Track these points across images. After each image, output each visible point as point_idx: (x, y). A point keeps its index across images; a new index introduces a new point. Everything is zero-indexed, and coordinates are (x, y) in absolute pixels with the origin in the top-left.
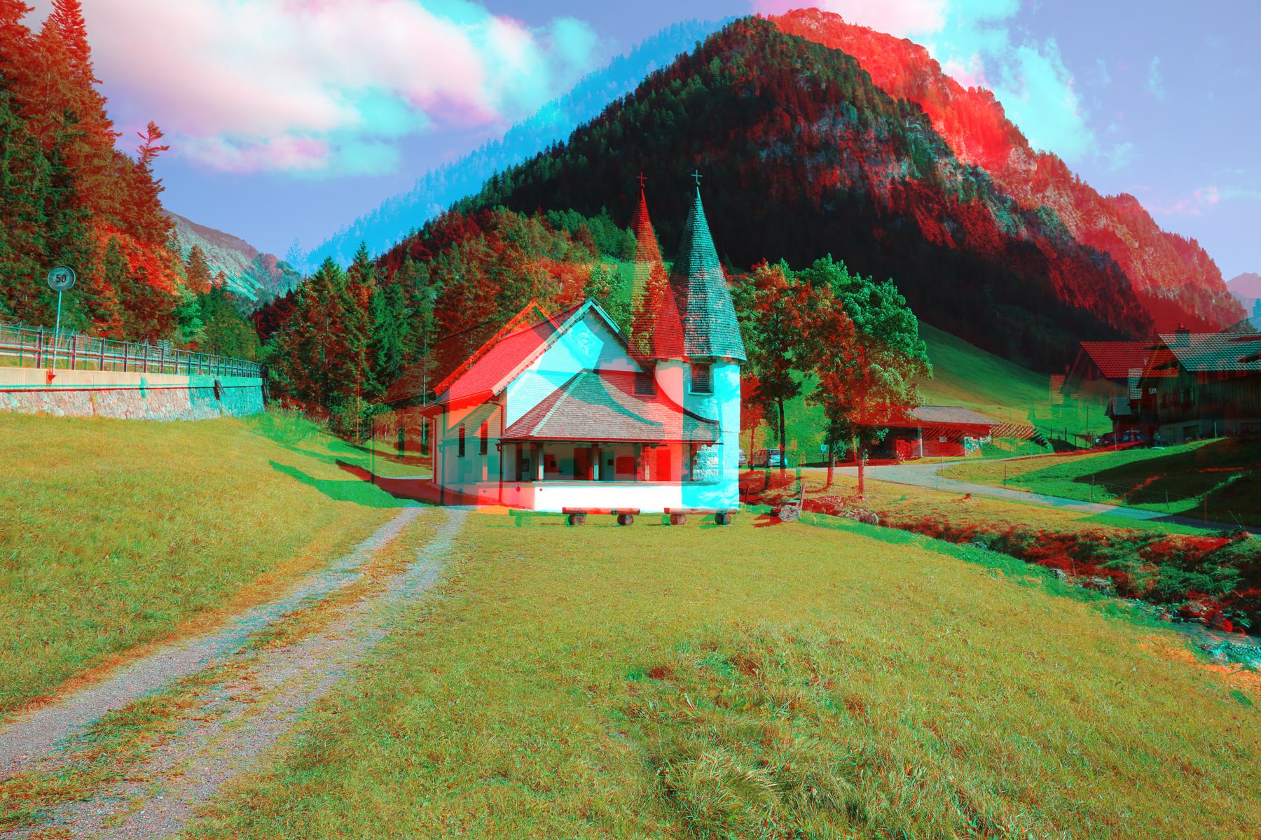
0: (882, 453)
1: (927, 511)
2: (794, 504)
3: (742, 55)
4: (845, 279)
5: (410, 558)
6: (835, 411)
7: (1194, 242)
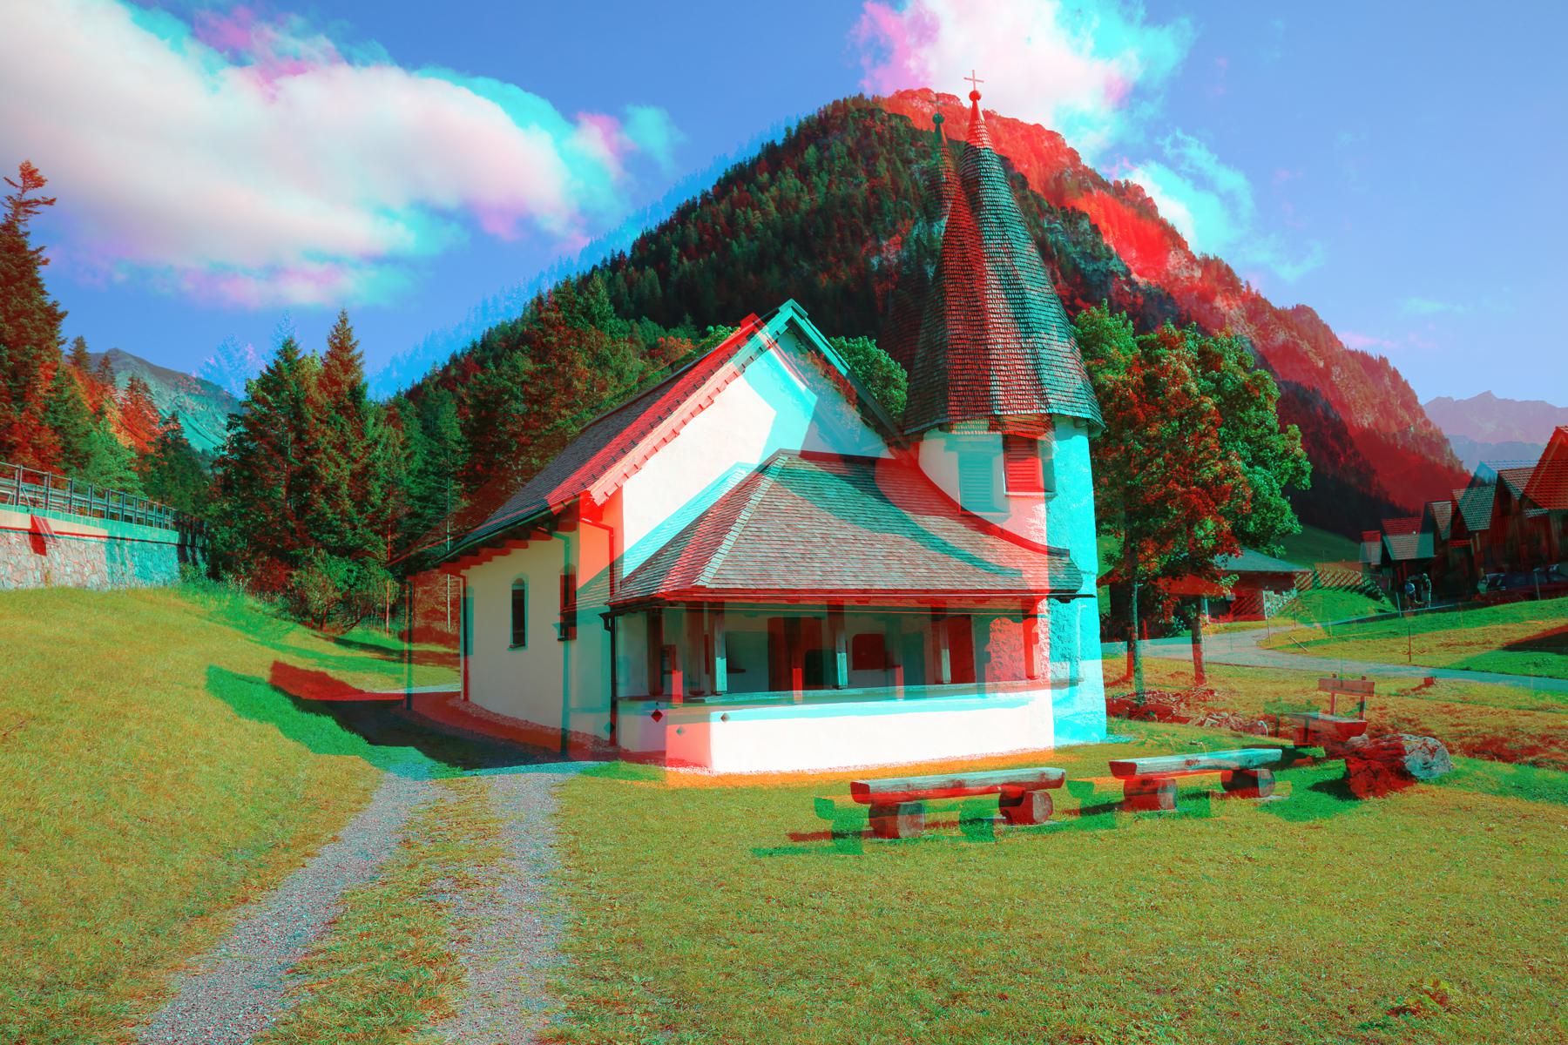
3: (843, 143)
7: (1384, 361)
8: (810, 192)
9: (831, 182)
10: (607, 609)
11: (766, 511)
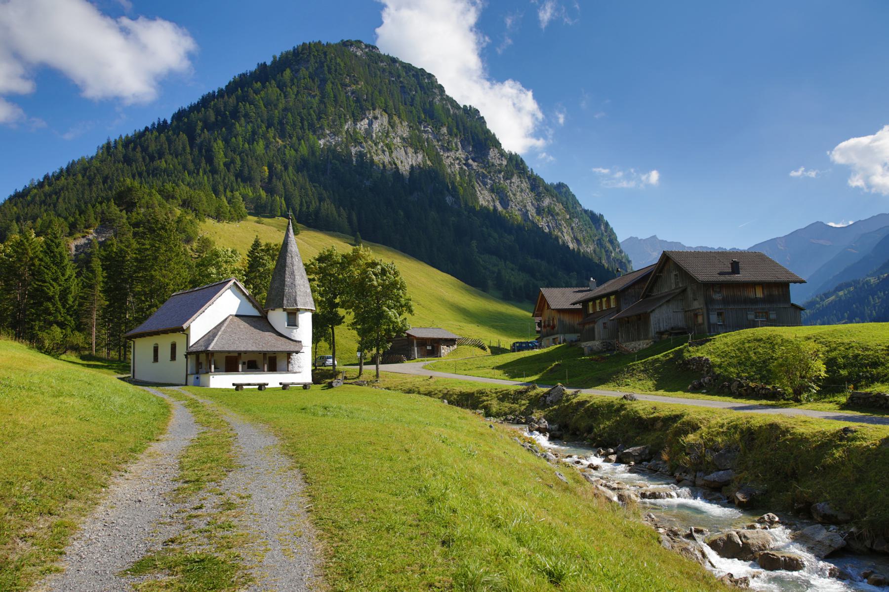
0: (391, 357)
3: (307, 69)
6: (362, 333)
7: (601, 216)
8: (285, 97)
9: (298, 92)
11: (225, 332)
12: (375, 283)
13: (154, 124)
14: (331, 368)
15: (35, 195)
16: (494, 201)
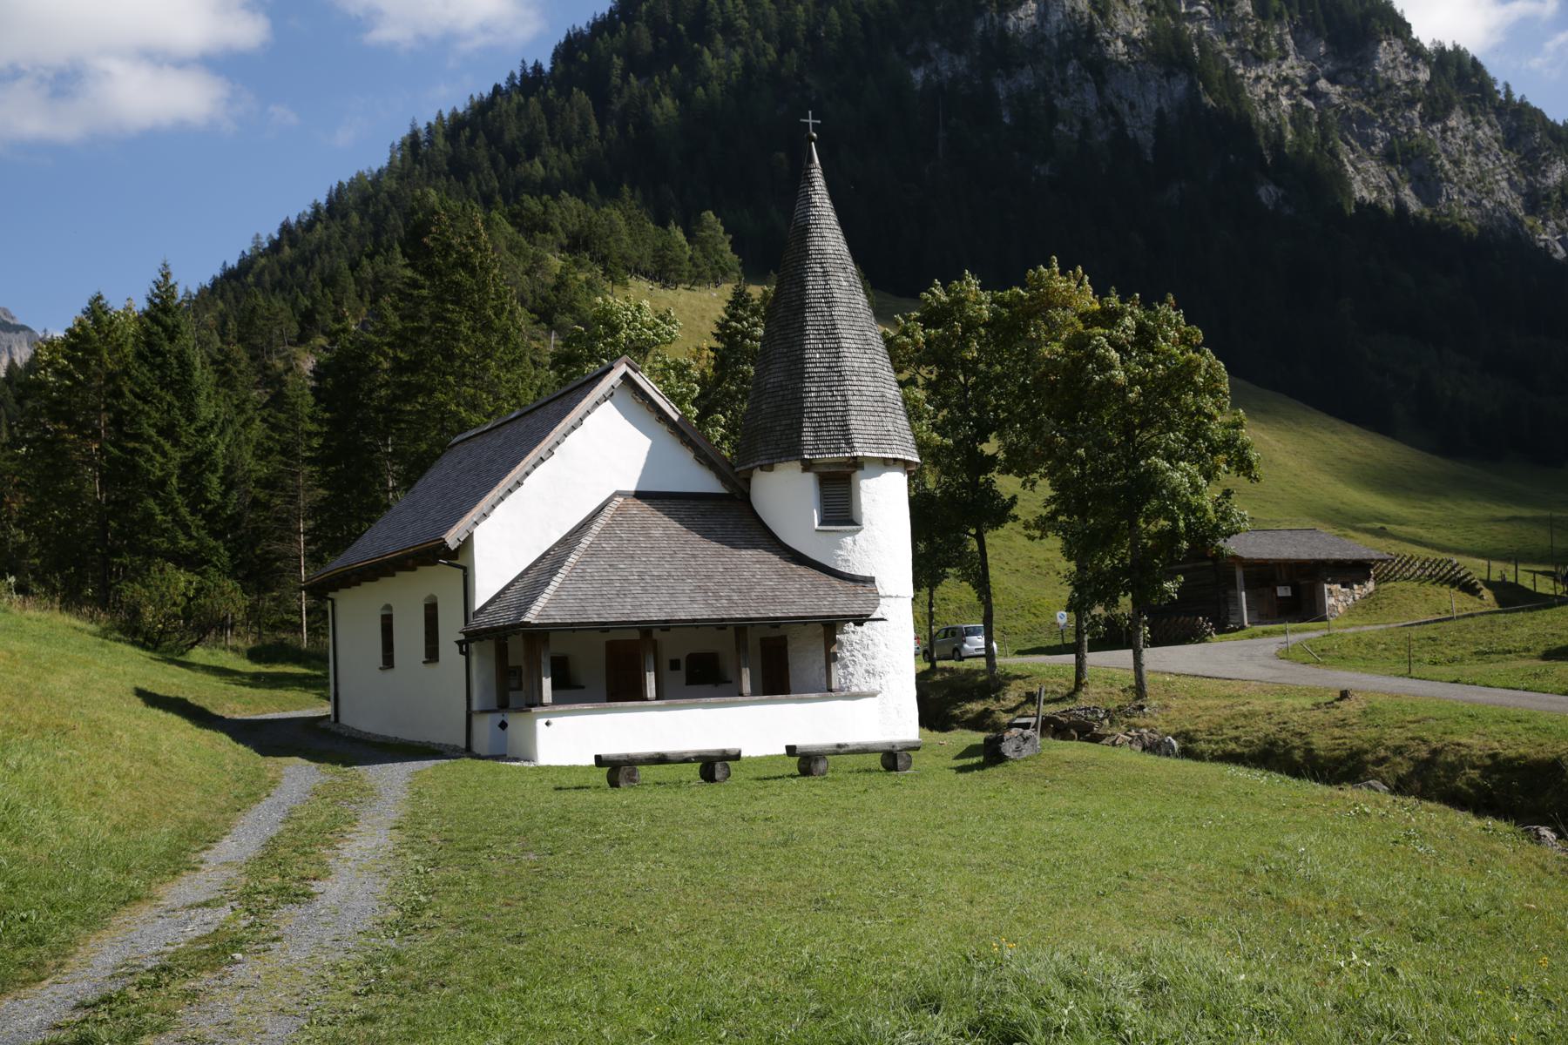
0: (1175, 626)
1: (1266, 728)
2: (1026, 726)
4: (1088, 301)
5: (311, 871)
6: (1080, 547)
10: (462, 637)
11: (593, 552)
12: (1120, 375)
13: (512, 76)
14: (981, 663)
15: (264, 267)
16: (1395, 187)
